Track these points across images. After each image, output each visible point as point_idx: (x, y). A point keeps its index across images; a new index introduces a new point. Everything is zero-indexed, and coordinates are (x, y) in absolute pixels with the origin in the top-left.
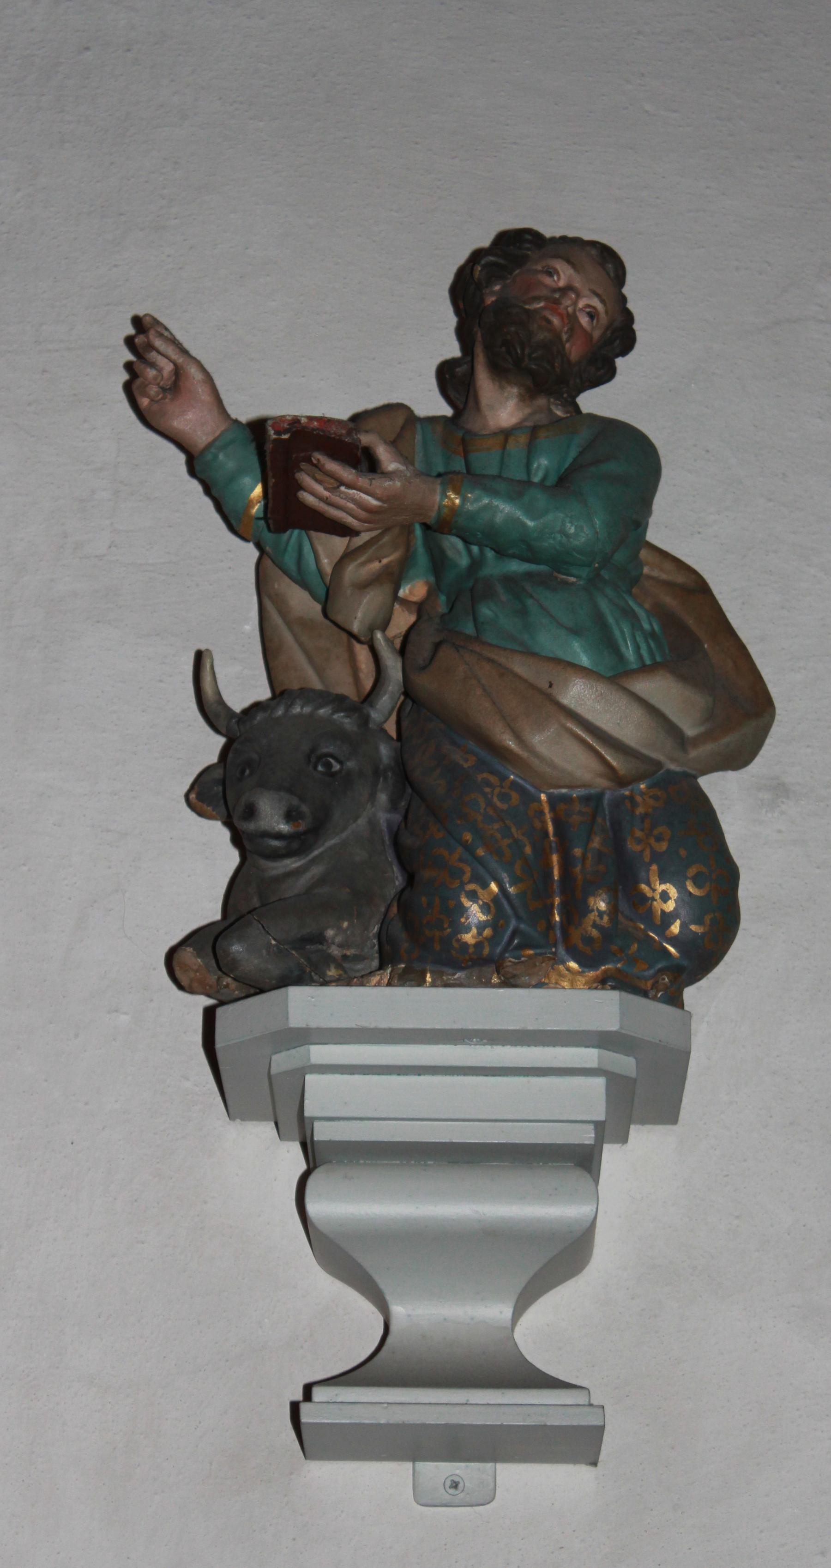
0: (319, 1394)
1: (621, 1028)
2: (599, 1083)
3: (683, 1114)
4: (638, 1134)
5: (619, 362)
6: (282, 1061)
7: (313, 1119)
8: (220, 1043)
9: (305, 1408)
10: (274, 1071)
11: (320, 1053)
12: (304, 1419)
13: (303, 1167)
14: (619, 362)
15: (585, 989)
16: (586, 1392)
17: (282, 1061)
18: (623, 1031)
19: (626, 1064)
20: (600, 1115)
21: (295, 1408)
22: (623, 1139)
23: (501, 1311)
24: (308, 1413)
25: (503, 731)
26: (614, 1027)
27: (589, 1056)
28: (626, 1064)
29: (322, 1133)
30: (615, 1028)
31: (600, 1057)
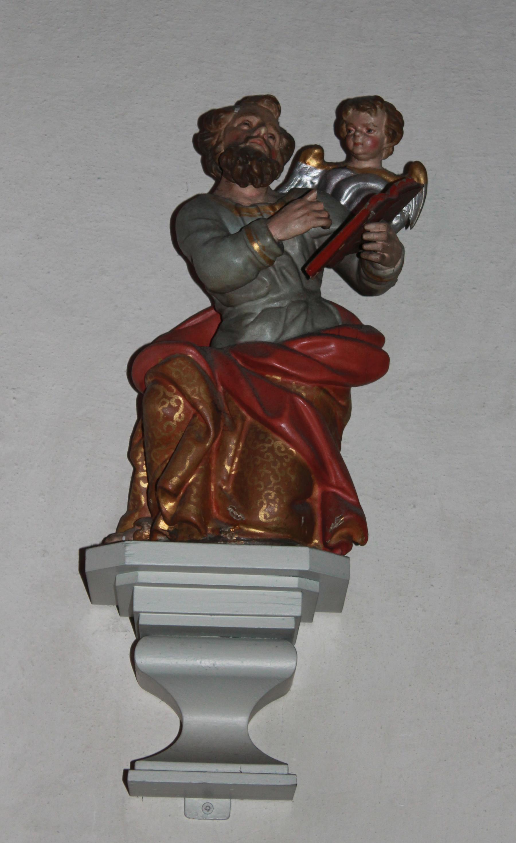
0: (138, 765)
1: (310, 568)
2: (299, 594)
3: (343, 611)
4: (319, 617)
5: (385, 348)
6: (122, 579)
7: (138, 613)
8: (87, 569)
9: (131, 774)
10: (118, 583)
11: (143, 576)
12: (130, 778)
13: (134, 638)
14: (385, 348)
15: (306, 232)
16: (286, 766)
17: (122, 579)
18: (311, 570)
19: (314, 585)
20: (298, 612)
21: (126, 773)
22: (310, 619)
23: (241, 720)
24: (132, 776)
25: (316, 156)
26: (307, 568)
27: (293, 581)
28: (314, 585)
29: (144, 620)
30: (307, 569)
31: (299, 582)
